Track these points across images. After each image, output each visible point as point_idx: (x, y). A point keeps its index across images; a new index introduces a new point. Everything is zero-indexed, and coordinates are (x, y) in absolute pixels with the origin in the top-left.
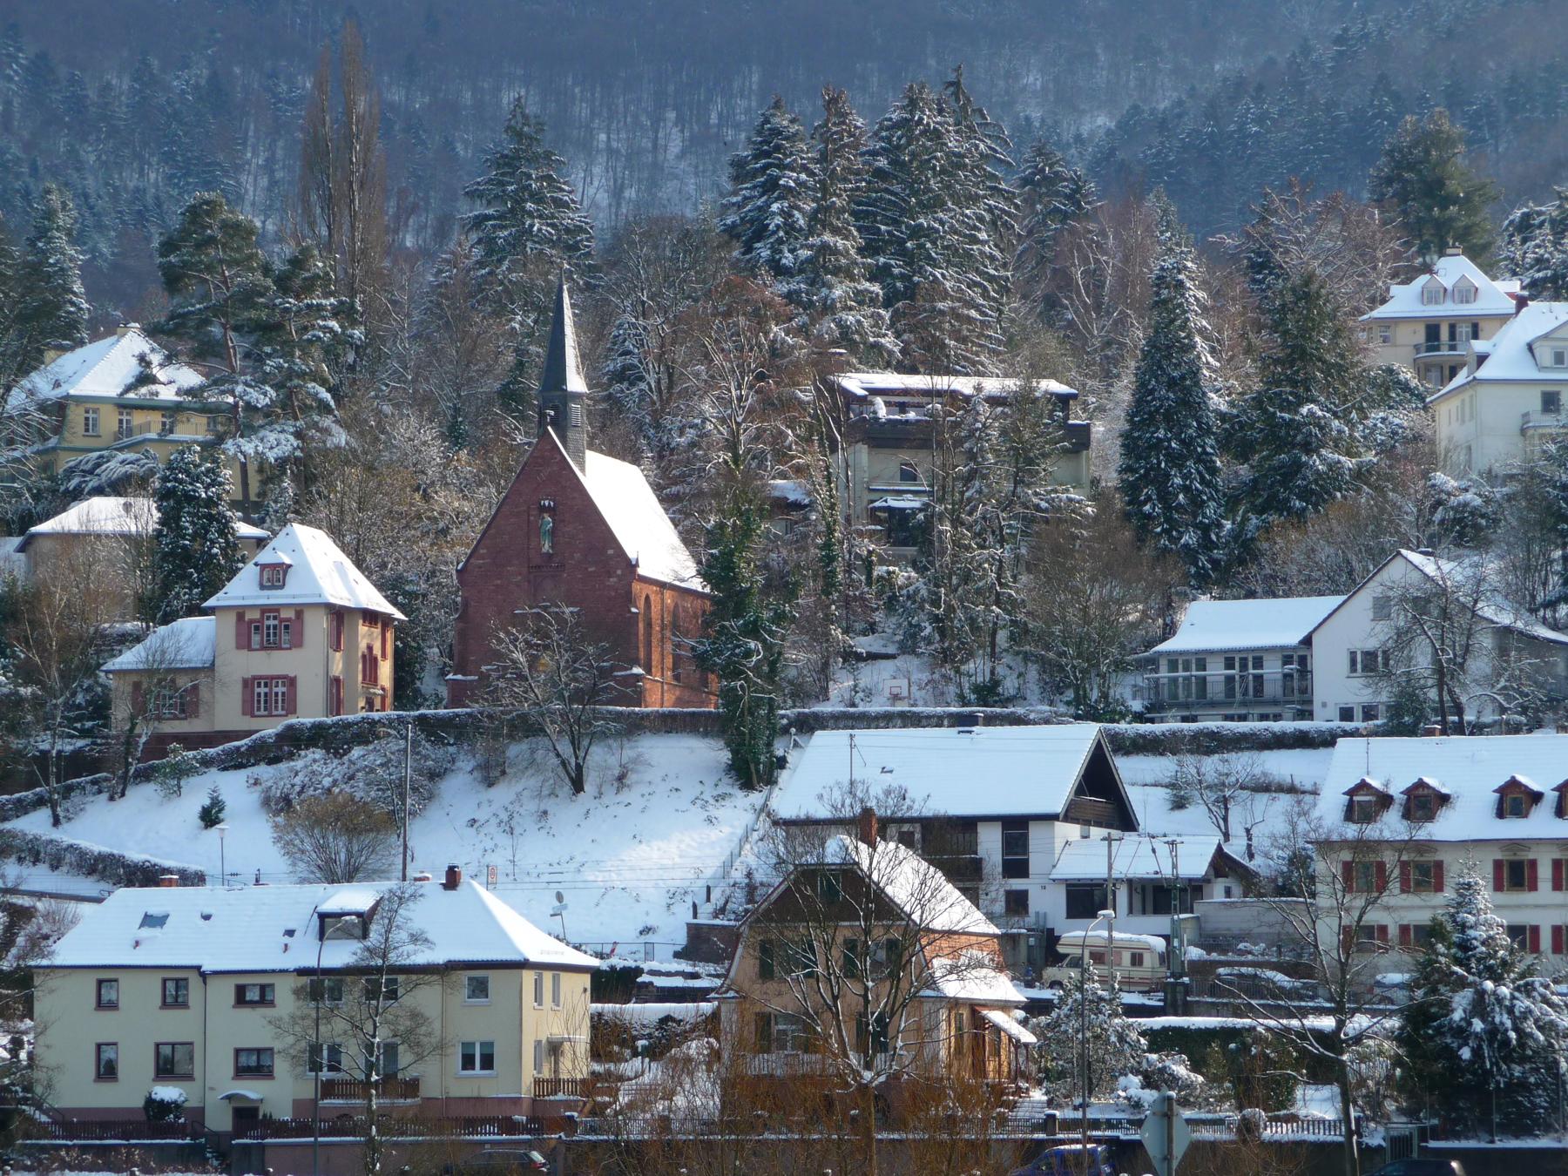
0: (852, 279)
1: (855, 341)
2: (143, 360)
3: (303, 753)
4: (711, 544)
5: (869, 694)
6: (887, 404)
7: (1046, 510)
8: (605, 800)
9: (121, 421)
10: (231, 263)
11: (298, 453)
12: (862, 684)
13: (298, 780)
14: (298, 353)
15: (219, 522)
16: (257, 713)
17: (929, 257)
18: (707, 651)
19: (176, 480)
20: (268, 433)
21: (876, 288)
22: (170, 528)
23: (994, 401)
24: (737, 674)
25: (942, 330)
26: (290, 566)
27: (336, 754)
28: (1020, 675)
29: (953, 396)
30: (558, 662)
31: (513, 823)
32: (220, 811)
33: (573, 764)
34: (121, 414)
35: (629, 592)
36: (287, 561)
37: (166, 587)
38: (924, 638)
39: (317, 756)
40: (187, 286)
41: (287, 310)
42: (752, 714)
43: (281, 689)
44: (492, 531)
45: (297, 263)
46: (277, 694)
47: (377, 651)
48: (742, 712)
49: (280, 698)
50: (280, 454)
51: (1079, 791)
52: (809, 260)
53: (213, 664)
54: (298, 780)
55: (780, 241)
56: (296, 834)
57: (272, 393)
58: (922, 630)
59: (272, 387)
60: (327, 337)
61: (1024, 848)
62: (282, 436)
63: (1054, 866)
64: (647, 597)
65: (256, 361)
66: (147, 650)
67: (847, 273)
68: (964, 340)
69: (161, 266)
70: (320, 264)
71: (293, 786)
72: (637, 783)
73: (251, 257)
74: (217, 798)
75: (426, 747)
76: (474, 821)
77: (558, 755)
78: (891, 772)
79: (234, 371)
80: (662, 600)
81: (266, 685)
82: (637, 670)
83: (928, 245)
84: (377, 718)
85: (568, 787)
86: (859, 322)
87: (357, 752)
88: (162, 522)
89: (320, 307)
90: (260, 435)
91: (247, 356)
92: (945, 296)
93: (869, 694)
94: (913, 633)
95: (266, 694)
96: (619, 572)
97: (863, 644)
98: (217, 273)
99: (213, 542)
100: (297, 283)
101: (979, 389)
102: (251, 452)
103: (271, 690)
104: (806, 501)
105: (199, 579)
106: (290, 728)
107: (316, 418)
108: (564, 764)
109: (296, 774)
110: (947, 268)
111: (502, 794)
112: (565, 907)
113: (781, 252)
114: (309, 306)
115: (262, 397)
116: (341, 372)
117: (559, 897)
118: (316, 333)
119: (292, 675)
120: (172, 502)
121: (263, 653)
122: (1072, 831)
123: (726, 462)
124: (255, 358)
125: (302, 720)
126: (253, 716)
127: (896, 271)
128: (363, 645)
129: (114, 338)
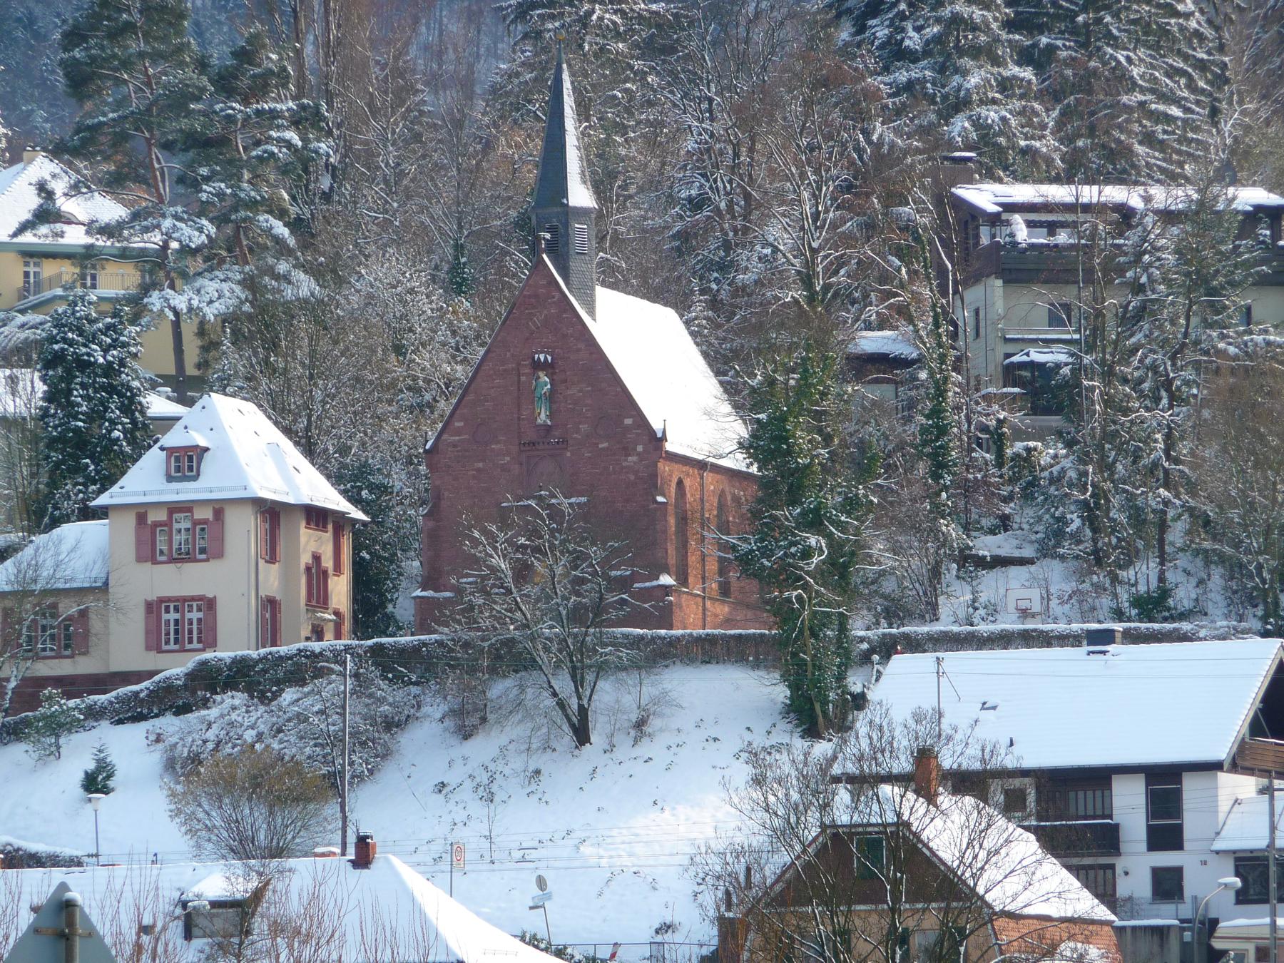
0: (997, 61)
1: (999, 145)
2: (43, 189)
3: (218, 698)
4: (756, 408)
5: (993, 611)
6: (1031, 224)
7: (1236, 358)
8: (618, 754)
9: (27, 274)
10: (156, 57)
11: (247, 308)
12: (983, 598)
13: (211, 735)
14: (247, 175)
15: (120, 395)
16: (165, 647)
17: (1109, 35)
18: (752, 551)
19: (65, 340)
20: (206, 282)
21: (1027, 73)
22: (59, 405)
23: (1168, 217)
24: (795, 580)
25: (1129, 133)
26: (207, 449)
27: (263, 699)
28: (1201, 582)
29: (1125, 214)
30: (552, 570)
31: (494, 788)
32: (109, 777)
33: (575, 707)
34: (27, 264)
35: (654, 475)
36: (202, 442)
37: (53, 484)
38: (1072, 535)
39: (237, 702)
40: (99, 91)
41: (230, 119)
42: (814, 635)
43: (195, 615)
44: (471, 397)
45: (245, 56)
46: (191, 623)
47: (328, 563)
48: (801, 632)
49: (195, 627)
50: (223, 309)
51: (1256, 728)
52: (938, 39)
53: (106, 584)
54: (211, 735)
55: (902, 16)
56: (200, 805)
57: (211, 229)
58: (1067, 524)
59: (211, 221)
60: (282, 154)
61: (1177, 811)
62: (225, 286)
63: (1218, 834)
64: (680, 483)
65: (192, 186)
66: (18, 566)
67: (986, 54)
68: (1162, 146)
69: (62, 63)
70: (274, 57)
71: (205, 742)
72: (661, 730)
73: (181, 49)
74: (104, 760)
75: (383, 688)
76: (443, 785)
77: (555, 694)
78: (994, 708)
79: (161, 201)
80: (702, 485)
81: (176, 609)
82: (666, 580)
83: (1108, 19)
84: (318, 650)
85: (568, 738)
86: (1003, 119)
87: (289, 695)
88: (49, 397)
89: (274, 114)
90: (197, 284)
91: (181, 180)
92: (1133, 86)
93: (993, 611)
94: (1058, 532)
95: (177, 622)
96: (640, 448)
97: (986, 545)
98: (139, 72)
99: (113, 423)
100: (244, 83)
101: (1147, 199)
102: (183, 307)
103: (183, 616)
104: (914, 355)
105: (98, 472)
106: (204, 663)
107: (271, 261)
108: (561, 705)
109: (209, 726)
110: (1135, 49)
111: (482, 748)
112: (549, 897)
113: (903, 30)
114: (259, 113)
115: (197, 233)
116: (312, 203)
117: (541, 883)
118: (269, 147)
119: (211, 596)
120: (60, 370)
121: (172, 566)
122: (1246, 786)
123: (796, 301)
124: (188, 182)
125: (219, 654)
126: (160, 651)
127: (1063, 54)
128: (306, 559)
129: (19, 166)
